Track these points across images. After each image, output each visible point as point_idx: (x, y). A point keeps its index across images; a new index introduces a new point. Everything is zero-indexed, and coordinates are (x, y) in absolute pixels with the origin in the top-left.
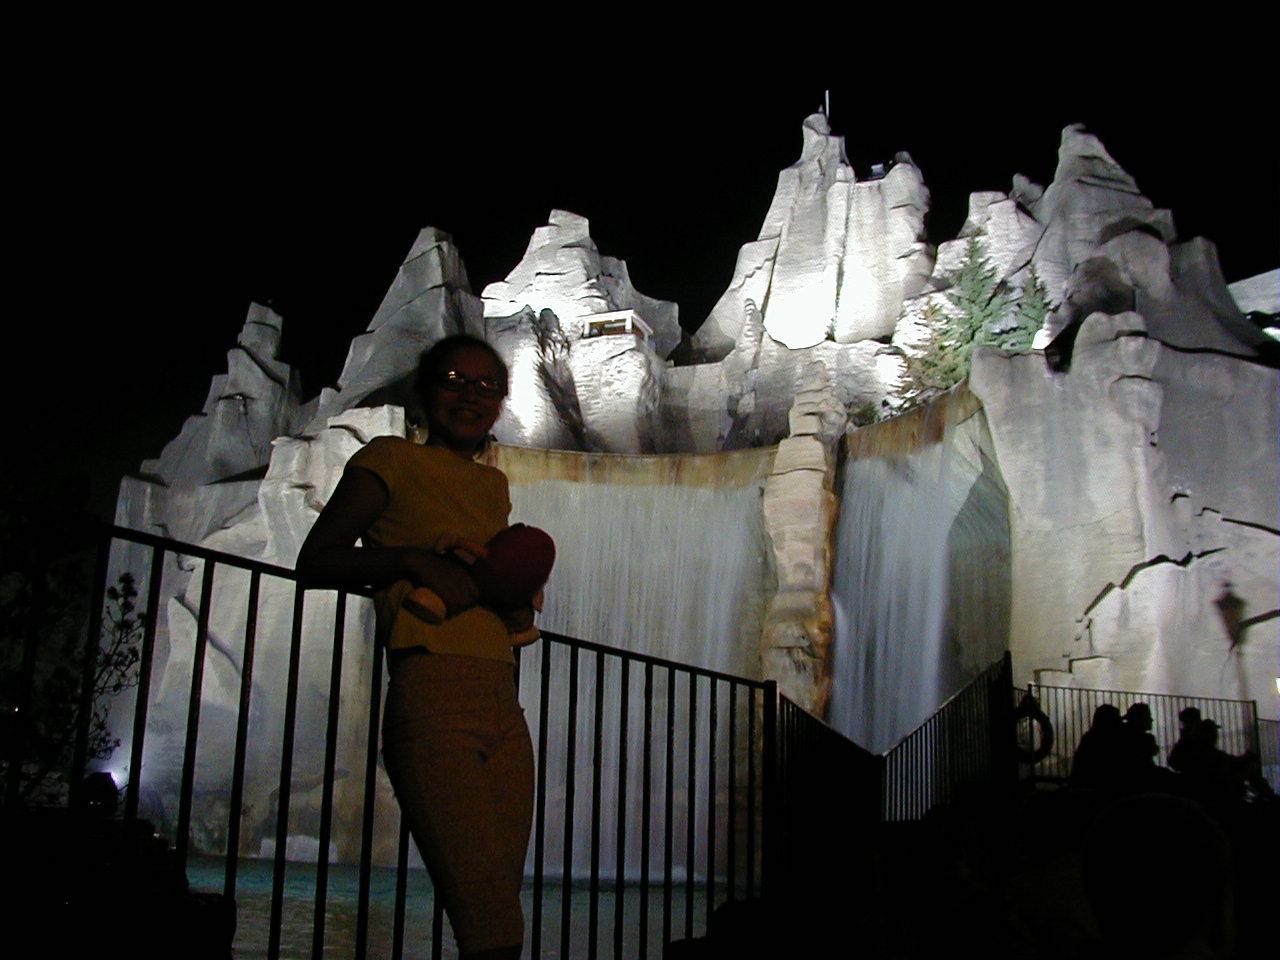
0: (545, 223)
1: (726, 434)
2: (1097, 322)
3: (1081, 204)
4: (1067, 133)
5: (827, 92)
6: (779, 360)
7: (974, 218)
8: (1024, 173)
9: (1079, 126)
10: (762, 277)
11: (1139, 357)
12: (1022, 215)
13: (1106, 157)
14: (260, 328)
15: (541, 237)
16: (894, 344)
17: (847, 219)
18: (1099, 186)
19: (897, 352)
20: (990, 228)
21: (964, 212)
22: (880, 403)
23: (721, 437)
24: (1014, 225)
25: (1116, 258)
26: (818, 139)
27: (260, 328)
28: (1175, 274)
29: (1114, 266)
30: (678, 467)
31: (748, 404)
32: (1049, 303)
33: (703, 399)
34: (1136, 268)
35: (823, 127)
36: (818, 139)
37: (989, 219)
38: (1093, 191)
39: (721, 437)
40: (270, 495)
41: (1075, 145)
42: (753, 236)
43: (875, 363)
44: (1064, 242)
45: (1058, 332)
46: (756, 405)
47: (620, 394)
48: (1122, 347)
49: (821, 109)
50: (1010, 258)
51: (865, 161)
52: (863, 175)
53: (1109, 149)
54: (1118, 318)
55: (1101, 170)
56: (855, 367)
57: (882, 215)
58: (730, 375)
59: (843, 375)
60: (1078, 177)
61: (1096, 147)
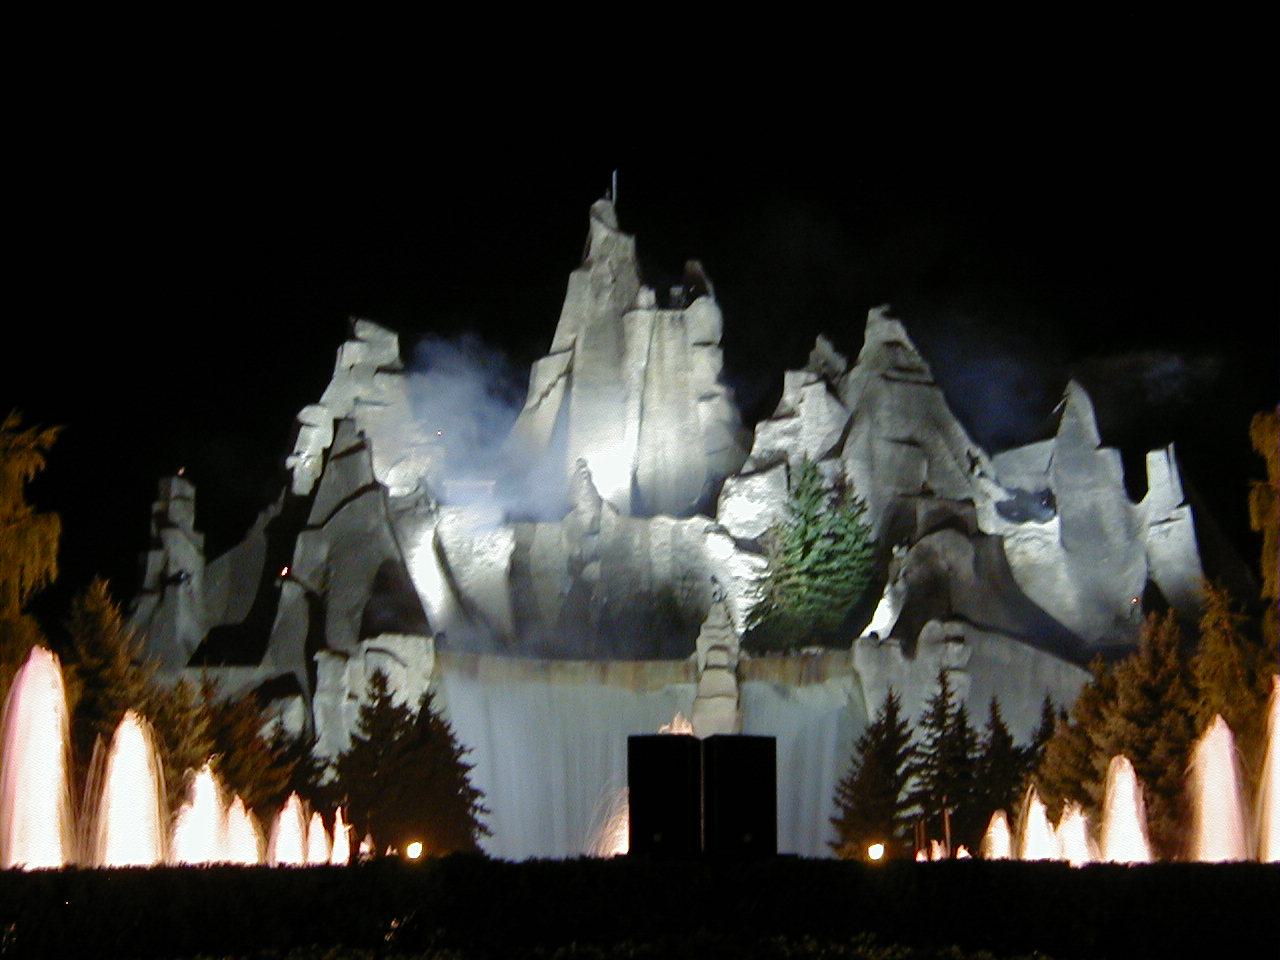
0: (353, 338)
1: (567, 590)
2: (933, 628)
3: (886, 403)
4: (874, 314)
5: (614, 174)
6: (618, 528)
7: (789, 397)
8: (829, 337)
9: (885, 308)
10: (556, 395)
11: (959, 655)
12: (831, 399)
13: (911, 347)
14: (180, 497)
15: (350, 354)
16: (720, 523)
17: (649, 350)
18: (905, 381)
19: (723, 531)
20: (803, 409)
21: (778, 390)
22: (709, 578)
23: (562, 594)
24: (824, 409)
25: (938, 547)
26: (607, 238)
27: (180, 497)
28: (977, 561)
29: (936, 554)
30: (604, 671)
31: (593, 570)
32: (855, 499)
33: (544, 557)
34: (952, 556)
35: (612, 220)
36: (607, 238)
37: (801, 401)
38: (896, 387)
39: (562, 594)
40: (329, 704)
41: (881, 329)
42: (544, 350)
43: (705, 540)
44: (870, 441)
45: (900, 610)
46: (602, 573)
47: (490, 565)
48: (949, 649)
49: (607, 194)
50: (820, 440)
51: (664, 275)
52: (663, 302)
53: (910, 334)
54: (947, 625)
55: (903, 360)
56: (687, 543)
57: (683, 349)
58: (570, 536)
59: (676, 549)
60: (883, 371)
61: (897, 331)
